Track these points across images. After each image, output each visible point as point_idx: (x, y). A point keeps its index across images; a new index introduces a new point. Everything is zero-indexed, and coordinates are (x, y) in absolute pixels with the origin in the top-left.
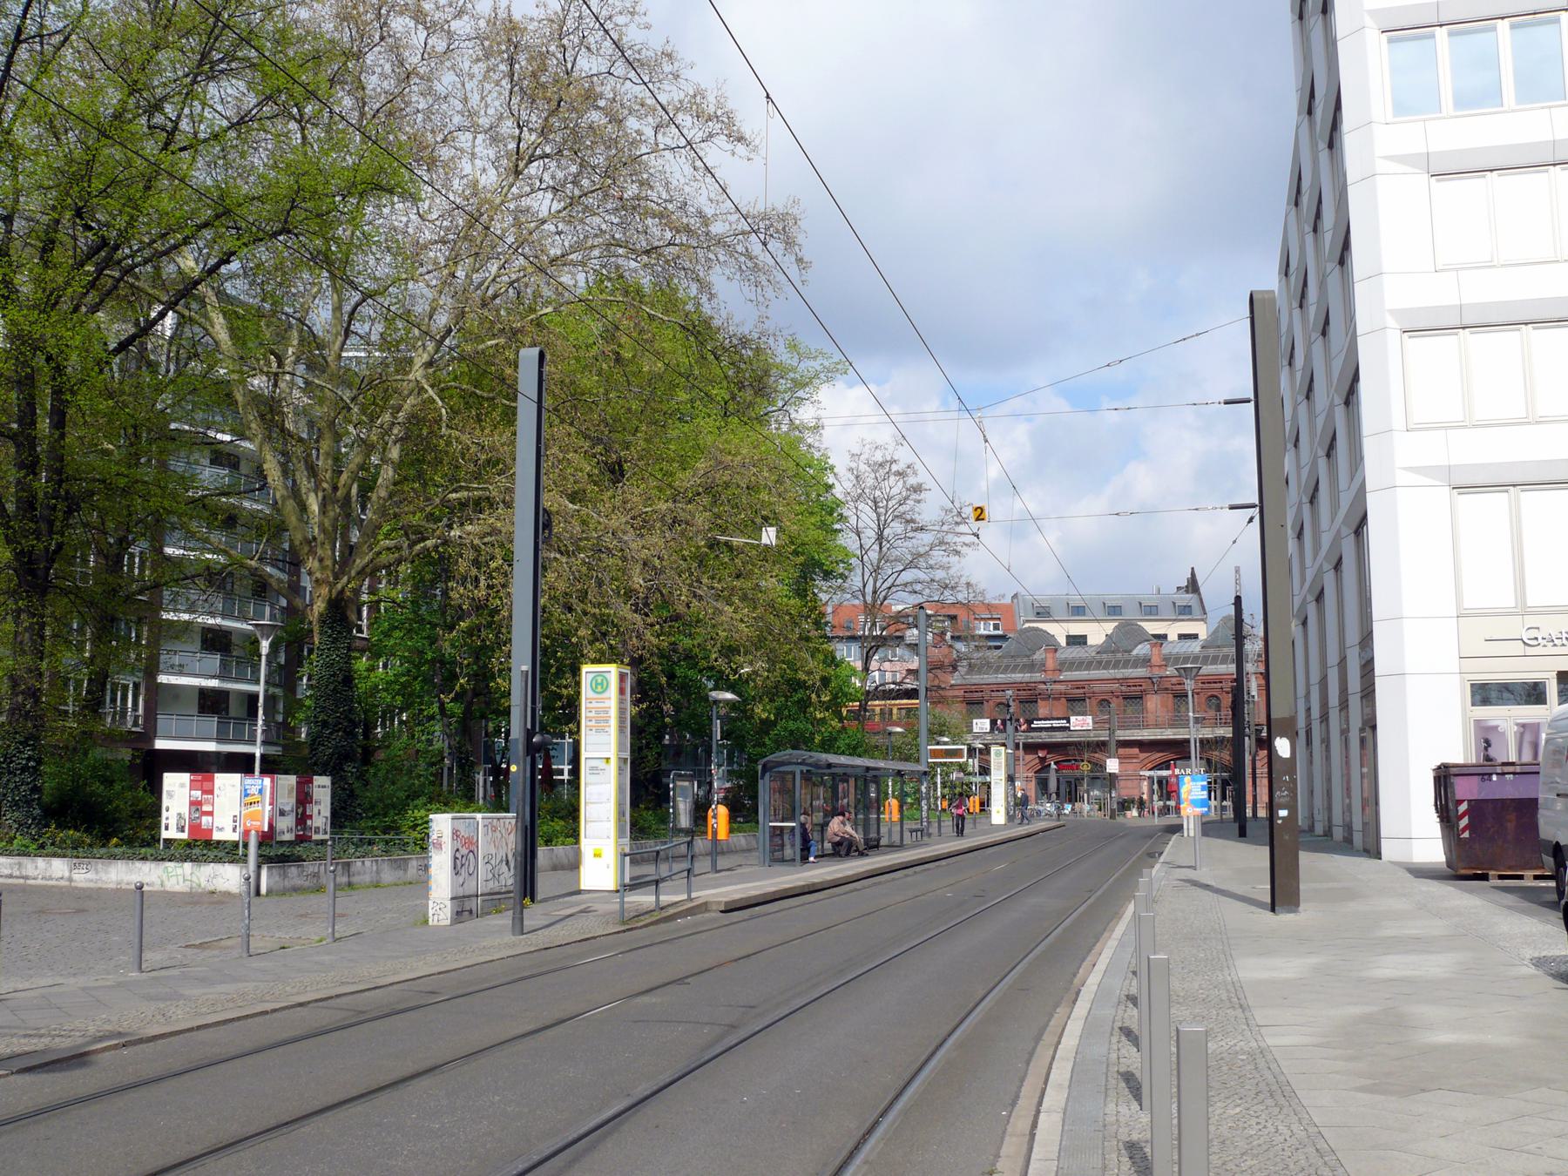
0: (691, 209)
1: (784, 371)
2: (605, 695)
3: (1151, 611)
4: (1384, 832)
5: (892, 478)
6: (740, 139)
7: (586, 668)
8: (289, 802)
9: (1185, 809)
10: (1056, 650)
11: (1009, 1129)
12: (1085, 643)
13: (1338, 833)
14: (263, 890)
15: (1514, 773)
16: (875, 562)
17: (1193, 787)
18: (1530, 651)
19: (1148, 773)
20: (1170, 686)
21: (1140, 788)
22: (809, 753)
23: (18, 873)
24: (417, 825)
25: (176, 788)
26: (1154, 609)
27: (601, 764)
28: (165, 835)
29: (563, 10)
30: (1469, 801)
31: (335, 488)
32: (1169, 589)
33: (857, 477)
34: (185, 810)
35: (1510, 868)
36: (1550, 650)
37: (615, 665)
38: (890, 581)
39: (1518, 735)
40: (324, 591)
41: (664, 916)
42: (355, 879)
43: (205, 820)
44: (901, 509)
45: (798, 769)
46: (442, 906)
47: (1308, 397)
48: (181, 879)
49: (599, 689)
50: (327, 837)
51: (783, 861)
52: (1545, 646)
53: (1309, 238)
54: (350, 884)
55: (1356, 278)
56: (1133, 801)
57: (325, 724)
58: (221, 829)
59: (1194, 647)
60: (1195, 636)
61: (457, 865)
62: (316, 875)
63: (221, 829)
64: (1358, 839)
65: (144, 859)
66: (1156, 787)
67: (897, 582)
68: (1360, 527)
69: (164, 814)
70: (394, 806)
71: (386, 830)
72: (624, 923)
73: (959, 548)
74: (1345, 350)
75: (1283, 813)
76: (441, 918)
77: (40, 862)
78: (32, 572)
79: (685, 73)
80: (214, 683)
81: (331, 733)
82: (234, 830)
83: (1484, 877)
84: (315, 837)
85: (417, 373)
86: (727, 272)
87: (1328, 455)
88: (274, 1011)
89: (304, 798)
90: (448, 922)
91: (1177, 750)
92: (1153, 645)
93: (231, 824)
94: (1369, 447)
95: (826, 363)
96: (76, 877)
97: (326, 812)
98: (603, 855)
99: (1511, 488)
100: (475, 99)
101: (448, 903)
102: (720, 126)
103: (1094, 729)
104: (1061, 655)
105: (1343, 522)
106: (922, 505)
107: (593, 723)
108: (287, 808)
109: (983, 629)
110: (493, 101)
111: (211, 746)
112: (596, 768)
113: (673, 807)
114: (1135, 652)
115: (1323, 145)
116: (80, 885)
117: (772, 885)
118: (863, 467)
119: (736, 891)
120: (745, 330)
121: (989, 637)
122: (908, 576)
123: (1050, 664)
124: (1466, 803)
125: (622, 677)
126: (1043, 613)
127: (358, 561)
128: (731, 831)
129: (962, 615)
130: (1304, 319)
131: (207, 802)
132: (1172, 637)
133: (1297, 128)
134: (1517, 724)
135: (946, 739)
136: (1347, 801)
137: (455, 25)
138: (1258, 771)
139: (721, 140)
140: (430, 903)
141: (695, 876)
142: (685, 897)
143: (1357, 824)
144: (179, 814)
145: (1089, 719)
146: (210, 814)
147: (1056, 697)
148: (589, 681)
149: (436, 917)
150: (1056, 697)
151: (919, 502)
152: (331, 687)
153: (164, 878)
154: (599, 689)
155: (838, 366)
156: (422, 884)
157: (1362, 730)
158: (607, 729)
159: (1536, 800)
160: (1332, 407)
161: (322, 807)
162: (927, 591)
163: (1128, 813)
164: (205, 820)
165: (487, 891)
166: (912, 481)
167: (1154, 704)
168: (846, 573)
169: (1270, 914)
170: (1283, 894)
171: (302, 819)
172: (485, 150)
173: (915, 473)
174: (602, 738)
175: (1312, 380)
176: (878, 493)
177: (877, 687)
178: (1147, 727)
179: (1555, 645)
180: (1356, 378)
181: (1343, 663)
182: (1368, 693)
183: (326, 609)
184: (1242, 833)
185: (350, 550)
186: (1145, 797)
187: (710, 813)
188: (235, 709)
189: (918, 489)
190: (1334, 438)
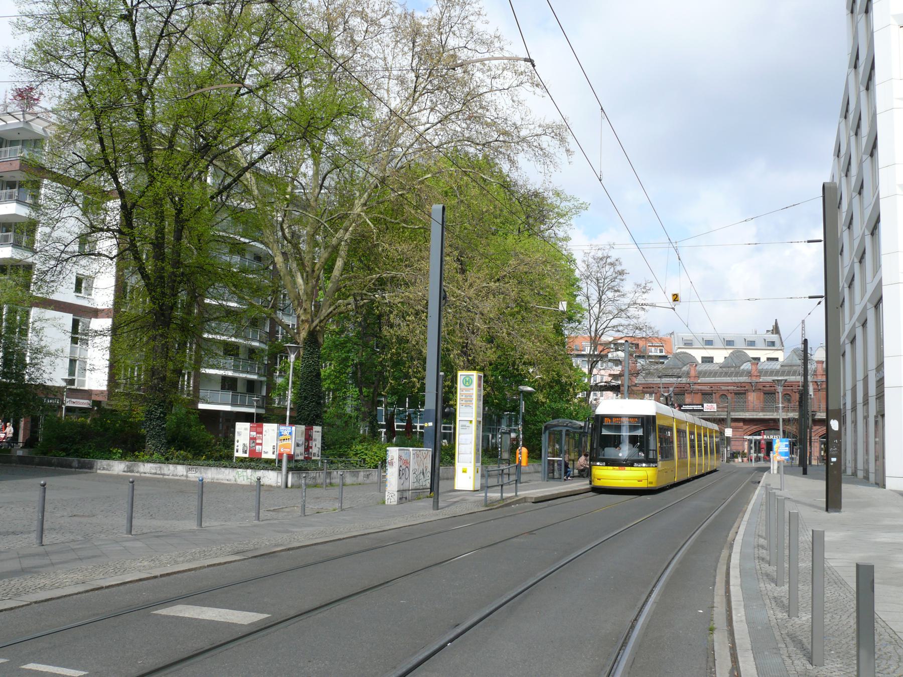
0: (510, 123)
1: (552, 207)
3: (752, 344)
4: (887, 473)
5: (607, 267)
7: (460, 373)
8: (302, 440)
10: (696, 365)
11: (715, 593)
12: (712, 362)
13: (860, 474)
14: (289, 485)
16: (597, 313)
17: (781, 446)
19: (748, 437)
21: (743, 446)
22: (570, 420)
23: (159, 472)
25: (242, 431)
27: (468, 424)
28: (236, 454)
29: (441, 12)
32: (762, 332)
33: (588, 265)
34: (247, 442)
38: (605, 325)
40: (307, 326)
41: (505, 504)
43: (258, 448)
44: (613, 284)
45: (564, 430)
47: (849, 228)
48: (245, 478)
49: (467, 384)
51: (553, 478)
53: (853, 138)
54: (331, 484)
56: (739, 453)
57: (306, 398)
58: (266, 453)
60: (777, 359)
61: (401, 473)
62: (314, 478)
63: (266, 453)
64: (872, 477)
65: (225, 467)
66: (753, 445)
67: (609, 325)
68: (878, 303)
69: (236, 444)
70: (344, 443)
71: (340, 456)
72: (486, 506)
74: (872, 205)
75: (834, 459)
77: (171, 466)
79: (506, 48)
80: (230, 373)
81: (309, 403)
82: (273, 453)
84: (313, 458)
85: (358, 209)
86: (528, 156)
87: (860, 262)
88: (344, 539)
89: (308, 438)
90: (396, 503)
91: (770, 425)
92: (752, 364)
93: (272, 450)
94: (884, 260)
95: (576, 204)
96: (190, 475)
97: (319, 445)
101: (396, 493)
102: (527, 77)
103: (718, 411)
104: (699, 368)
105: (869, 301)
106: (624, 282)
107: (463, 402)
108: (300, 443)
109: (654, 352)
110: (404, 60)
111: (228, 408)
112: (465, 426)
115: (863, 88)
116: (192, 479)
117: (557, 490)
118: (591, 260)
119: (537, 492)
121: (656, 356)
122: (615, 322)
123: (693, 373)
125: (480, 377)
126: (688, 344)
127: (324, 311)
128: (528, 462)
129: (641, 344)
130: (848, 183)
131: (259, 438)
132: (763, 359)
133: (848, 76)
136: (866, 457)
139: (527, 86)
140: (387, 493)
141: (521, 483)
142: (514, 494)
143: (872, 468)
144: (244, 444)
145: (715, 405)
146: (261, 444)
147: (696, 392)
150: (696, 392)
151: (622, 280)
152: (309, 378)
153: (237, 477)
154: (467, 384)
155: (583, 206)
156: (382, 483)
157: (876, 417)
160: (863, 235)
161: (317, 443)
162: (626, 330)
163: (736, 460)
164: (258, 448)
165: (414, 488)
166: (619, 268)
167: (753, 398)
168: (581, 319)
169: (826, 513)
170: (833, 502)
171: (307, 449)
172: (394, 87)
173: (620, 264)
174: (467, 410)
175: (852, 218)
176: (599, 275)
178: (748, 411)
180: (878, 220)
181: (866, 379)
182: (880, 397)
183: (307, 336)
184: (805, 472)
186: (746, 451)
187: (518, 451)
188: (241, 387)
189: (621, 273)
190: (864, 252)
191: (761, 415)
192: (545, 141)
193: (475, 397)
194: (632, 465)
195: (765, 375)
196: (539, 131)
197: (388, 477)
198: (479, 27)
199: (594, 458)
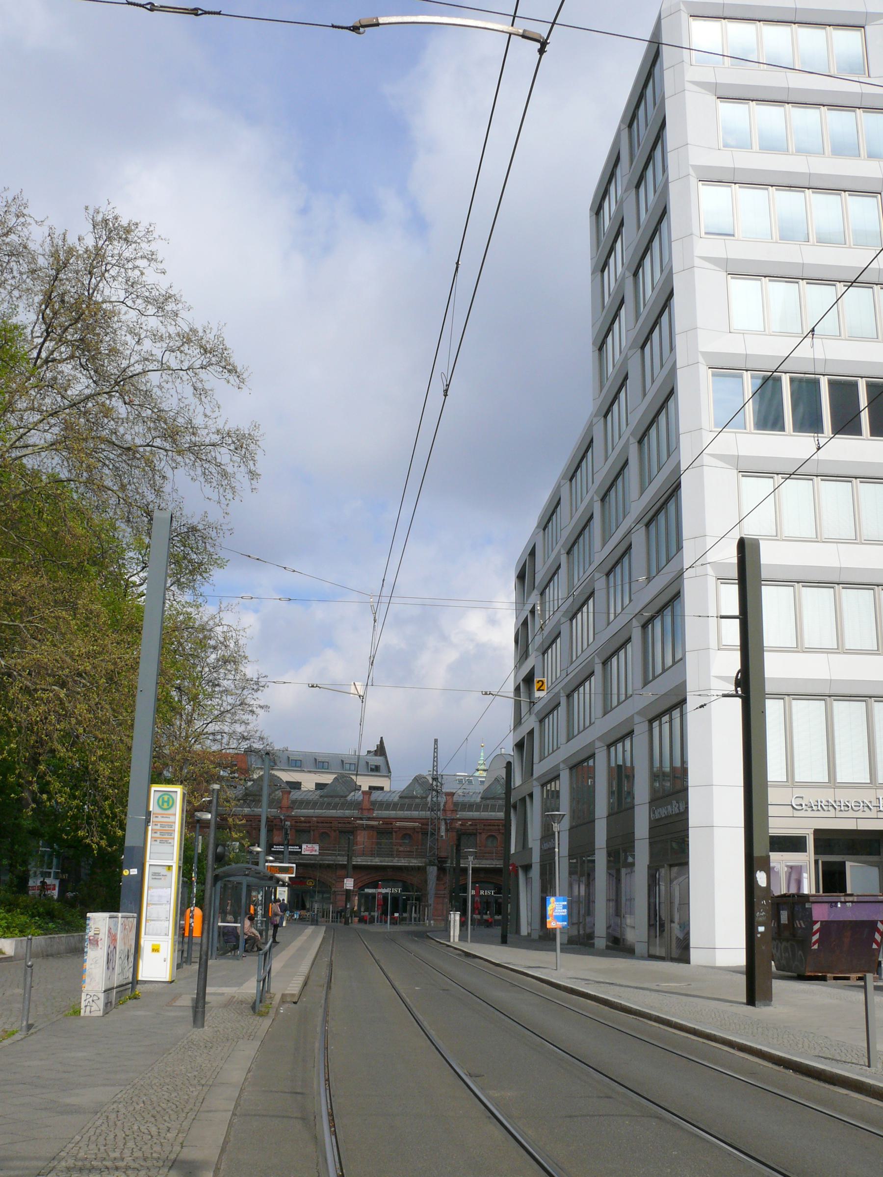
2: (171, 811)
6: (233, 371)
9: (550, 923)
12: (300, 788)
15: (852, 902)
18: (797, 814)
26: (298, 764)
27: (164, 871)
30: (822, 922)
35: (841, 972)
36: (810, 813)
37: (181, 786)
39: (788, 874)
46: (95, 998)
49: (165, 806)
52: (806, 810)
55: (684, 538)
60: (382, 788)
73: (255, 709)
75: (761, 929)
76: (93, 1009)
83: (823, 979)
90: (101, 1013)
98: (161, 950)
99: (786, 697)
101: (102, 996)
107: (158, 835)
112: (159, 874)
114: (349, 798)
120: (194, 521)
124: (819, 923)
134: (787, 866)
135: (271, 858)
140: (84, 997)
148: (157, 798)
149: (88, 1009)
154: (165, 806)
156: (79, 975)
158: (170, 841)
159: (118, 911)
169: (750, 1008)
174: (165, 848)
179: (813, 810)
191: (376, 861)
192: (224, 455)
193: (177, 827)
195: (463, 810)
196: (216, 438)
197: (88, 965)
198: (151, 277)
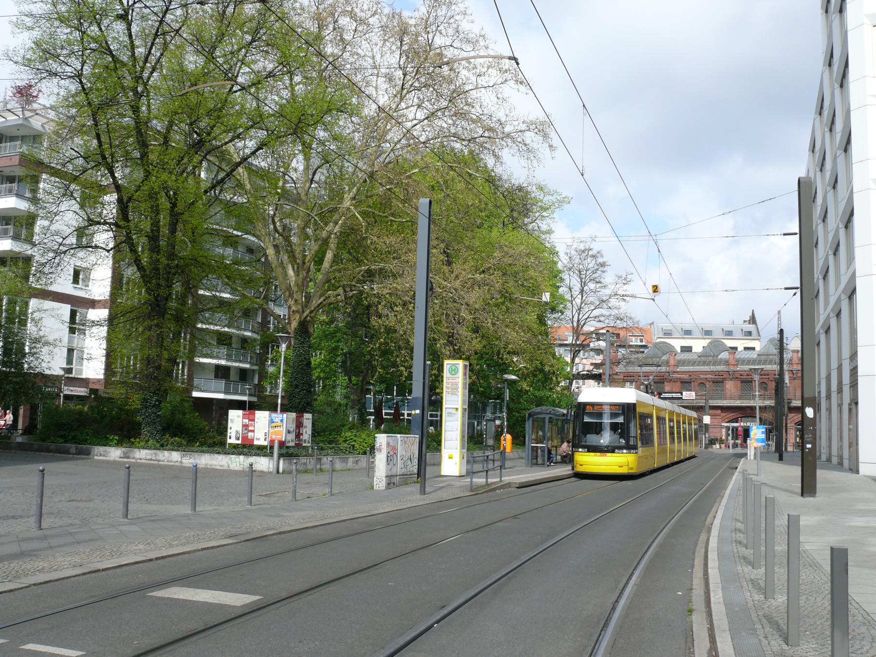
0: (494, 119)
1: (536, 201)
3: (729, 333)
4: (861, 459)
5: (589, 259)
7: (446, 362)
8: (293, 427)
10: (675, 355)
11: (694, 576)
12: (691, 351)
13: (835, 460)
14: (281, 470)
16: (579, 304)
17: (757, 432)
19: (726, 425)
20: (739, 377)
21: (721, 432)
22: (553, 408)
23: (154, 458)
24: (346, 440)
25: (235, 418)
27: (454, 411)
28: (229, 441)
29: (428, 12)
31: (304, 263)
32: (739, 322)
33: (570, 258)
34: (240, 429)
38: (587, 315)
41: (490, 489)
42: (323, 467)
43: (250, 435)
44: (595, 275)
45: (547, 417)
47: (824, 221)
48: (238, 464)
49: (453, 373)
50: (310, 445)
51: (537, 464)
53: (827, 134)
54: (321, 469)
56: (717, 440)
57: (297, 386)
58: (258, 439)
59: (753, 355)
60: (753, 349)
61: (389, 459)
62: (305, 464)
63: (258, 439)
64: (846, 463)
65: (219, 453)
66: (730, 432)
67: (591, 316)
68: (852, 294)
69: (229, 431)
70: (334, 430)
71: (330, 442)
72: (472, 491)
74: (846, 199)
75: (809, 446)
77: (166, 453)
78: (158, 305)
79: (491, 46)
80: (223, 362)
82: (265, 440)
84: (304, 445)
85: (347, 203)
86: (512, 151)
87: (835, 254)
88: (333, 523)
89: (299, 425)
90: (384, 488)
91: (747, 412)
92: (730, 353)
93: (264, 437)
94: (858, 252)
95: (559, 198)
96: (184, 461)
97: (310, 432)
100: (378, 57)
101: (384, 479)
102: (511, 75)
103: (696, 399)
104: (678, 357)
105: (843, 292)
106: (606, 274)
107: (450, 390)
108: (291, 430)
109: (634, 342)
110: (392, 59)
112: (451, 413)
113: (486, 434)
115: (837, 86)
116: (186, 465)
117: (540, 475)
118: (573, 252)
119: (521, 478)
122: (596, 312)
123: (672, 362)
125: (465, 366)
126: (668, 334)
127: (314, 301)
128: (512, 448)
129: (622, 333)
130: (823, 177)
131: (251, 425)
132: (740, 349)
133: (822, 74)
136: (840, 444)
137: (372, 21)
138: (788, 425)
139: (512, 83)
140: (375, 478)
141: (505, 469)
142: (499, 479)
143: (846, 454)
144: (237, 431)
145: (693, 393)
146: (253, 431)
147: (675, 381)
150: (675, 381)
151: (604, 272)
152: (300, 367)
153: (230, 463)
154: (453, 373)
156: (370, 469)
157: (850, 404)
160: (838, 228)
161: (307, 430)
162: (607, 320)
163: (714, 446)
164: (250, 435)
165: (401, 473)
166: (600, 260)
167: (730, 386)
168: (563, 310)
169: (801, 498)
170: (808, 487)
171: (298, 435)
174: (453, 398)
175: (826, 212)
177: (578, 373)
178: (726, 399)
180: (852, 214)
181: (840, 368)
182: (854, 385)
183: (298, 326)
184: (781, 458)
185: (308, 297)
186: (724, 438)
187: (502, 438)
188: (234, 376)
189: (603, 265)
190: (838, 245)
191: (738, 403)
192: (529, 137)
193: (460, 385)
194: (613, 452)
195: (742, 364)
196: (523, 127)
197: (377, 462)
198: (465, 26)
199: (576, 444)
